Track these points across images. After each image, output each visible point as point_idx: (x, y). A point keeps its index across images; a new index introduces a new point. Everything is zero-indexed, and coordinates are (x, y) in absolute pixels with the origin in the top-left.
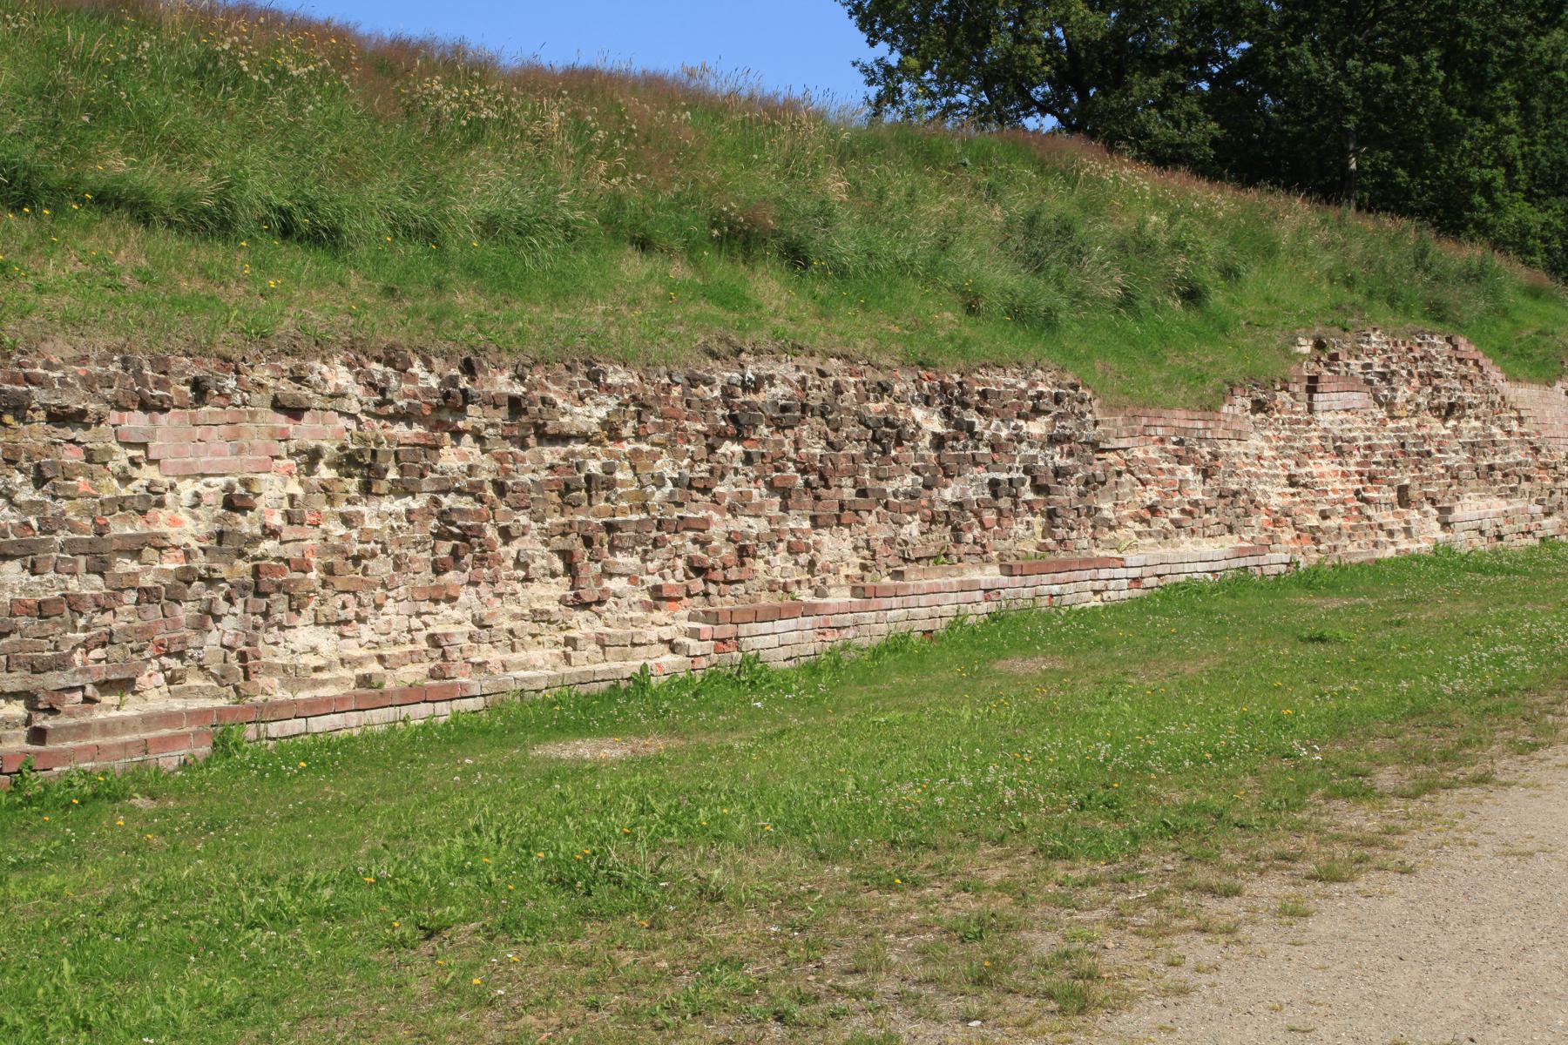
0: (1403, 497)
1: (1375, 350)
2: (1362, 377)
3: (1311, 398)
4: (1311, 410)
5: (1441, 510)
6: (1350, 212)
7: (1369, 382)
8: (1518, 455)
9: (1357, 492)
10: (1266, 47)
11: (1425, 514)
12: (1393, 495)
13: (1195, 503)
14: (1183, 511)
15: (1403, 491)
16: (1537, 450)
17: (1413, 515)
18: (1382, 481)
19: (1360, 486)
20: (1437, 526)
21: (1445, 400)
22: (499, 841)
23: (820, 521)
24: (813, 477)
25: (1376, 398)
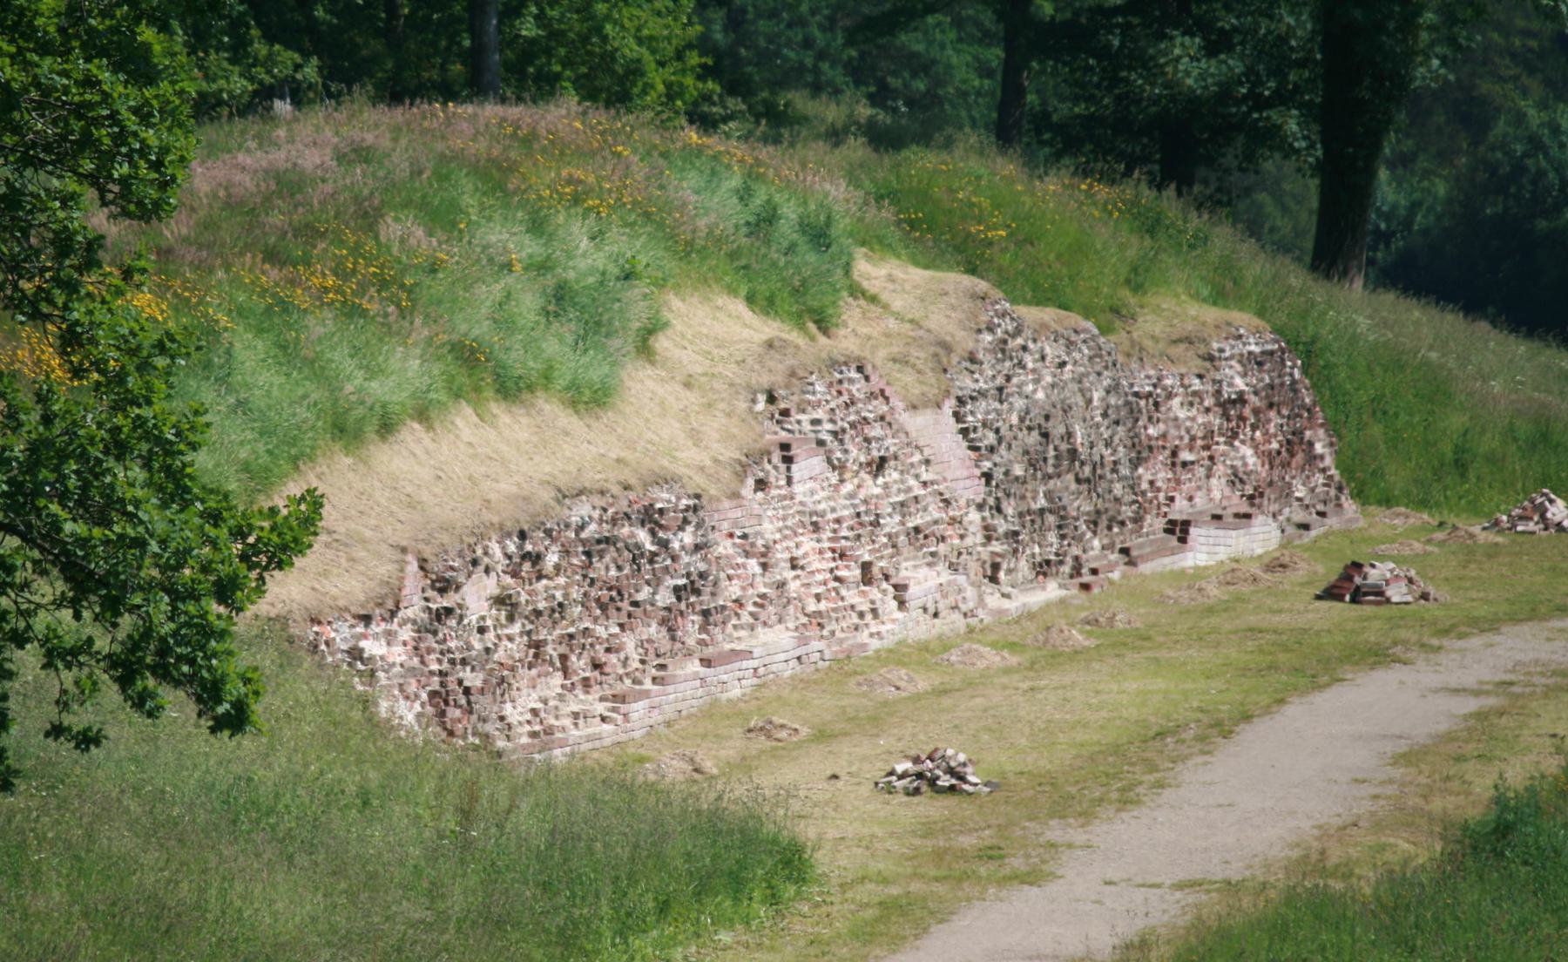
0: (867, 575)
1: (819, 402)
2: (812, 435)
3: (789, 469)
4: (789, 481)
5: (896, 587)
6: (1288, 261)
7: (821, 443)
8: (935, 512)
9: (832, 571)
10: (532, 42)
11: (884, 592)
12: (858, 572)
13: (763, 596)
14: (755, 604)
15: (866, 567)
16: (947, 502)
17: (874, 593)
18: (851, 558)
19: (833, 565)
20: (894, 604)
21: (875, 454)
22: (1529, 673)
23: (1134, 553)
24: (614, 593)
25: (829, 461)
